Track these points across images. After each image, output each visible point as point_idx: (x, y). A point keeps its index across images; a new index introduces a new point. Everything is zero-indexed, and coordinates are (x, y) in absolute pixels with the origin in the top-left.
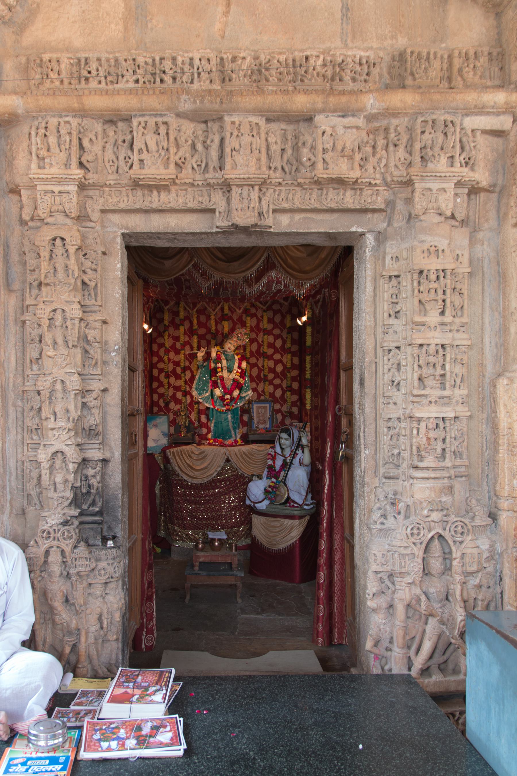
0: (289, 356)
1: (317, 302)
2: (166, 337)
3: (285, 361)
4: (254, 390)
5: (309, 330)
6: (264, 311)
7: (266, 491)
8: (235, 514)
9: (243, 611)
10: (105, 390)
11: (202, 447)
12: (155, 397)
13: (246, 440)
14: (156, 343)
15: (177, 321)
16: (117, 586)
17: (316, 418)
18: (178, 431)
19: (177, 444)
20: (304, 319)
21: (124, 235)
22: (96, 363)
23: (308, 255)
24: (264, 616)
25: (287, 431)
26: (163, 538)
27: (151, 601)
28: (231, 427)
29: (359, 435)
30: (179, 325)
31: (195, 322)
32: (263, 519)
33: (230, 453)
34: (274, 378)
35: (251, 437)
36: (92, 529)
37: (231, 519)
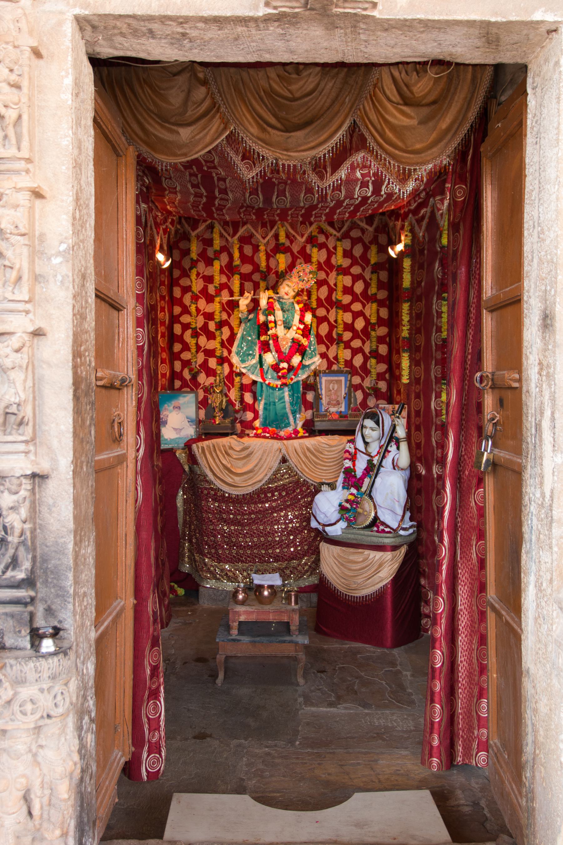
0: (375, 306)
1: (419, 221)
2: (193, 277)
3: (367, 314)
4: (323, 356)
5: (407, 263)
6: (338, 240)
7: (342, 508)
8: (294, 539)
9: (308, 701)
10: (38, 333)
11: (246, 440)
12: (178, 366)
13: (311, 429)
14: (179, 285)
15: (210, 253)
16: (64, 727)
17: (418, 396)
18: (210, 416)
19: (209, 436)
20: (400, 247)
21: (83, 23)
22: (19, 278)
23: (421, 123)
24: (340, 710)
25: (374, 417)
26: (188, 575)
27: (157, 698)
28: (288, 410)
29: (538, 427)
30: (212, 260)
31: (236, 255)
32: (336, 550)
33: (287, 449)
34: (352, 339)
35: (319, 426)
36: (12, 616)
37: (288, 546)
